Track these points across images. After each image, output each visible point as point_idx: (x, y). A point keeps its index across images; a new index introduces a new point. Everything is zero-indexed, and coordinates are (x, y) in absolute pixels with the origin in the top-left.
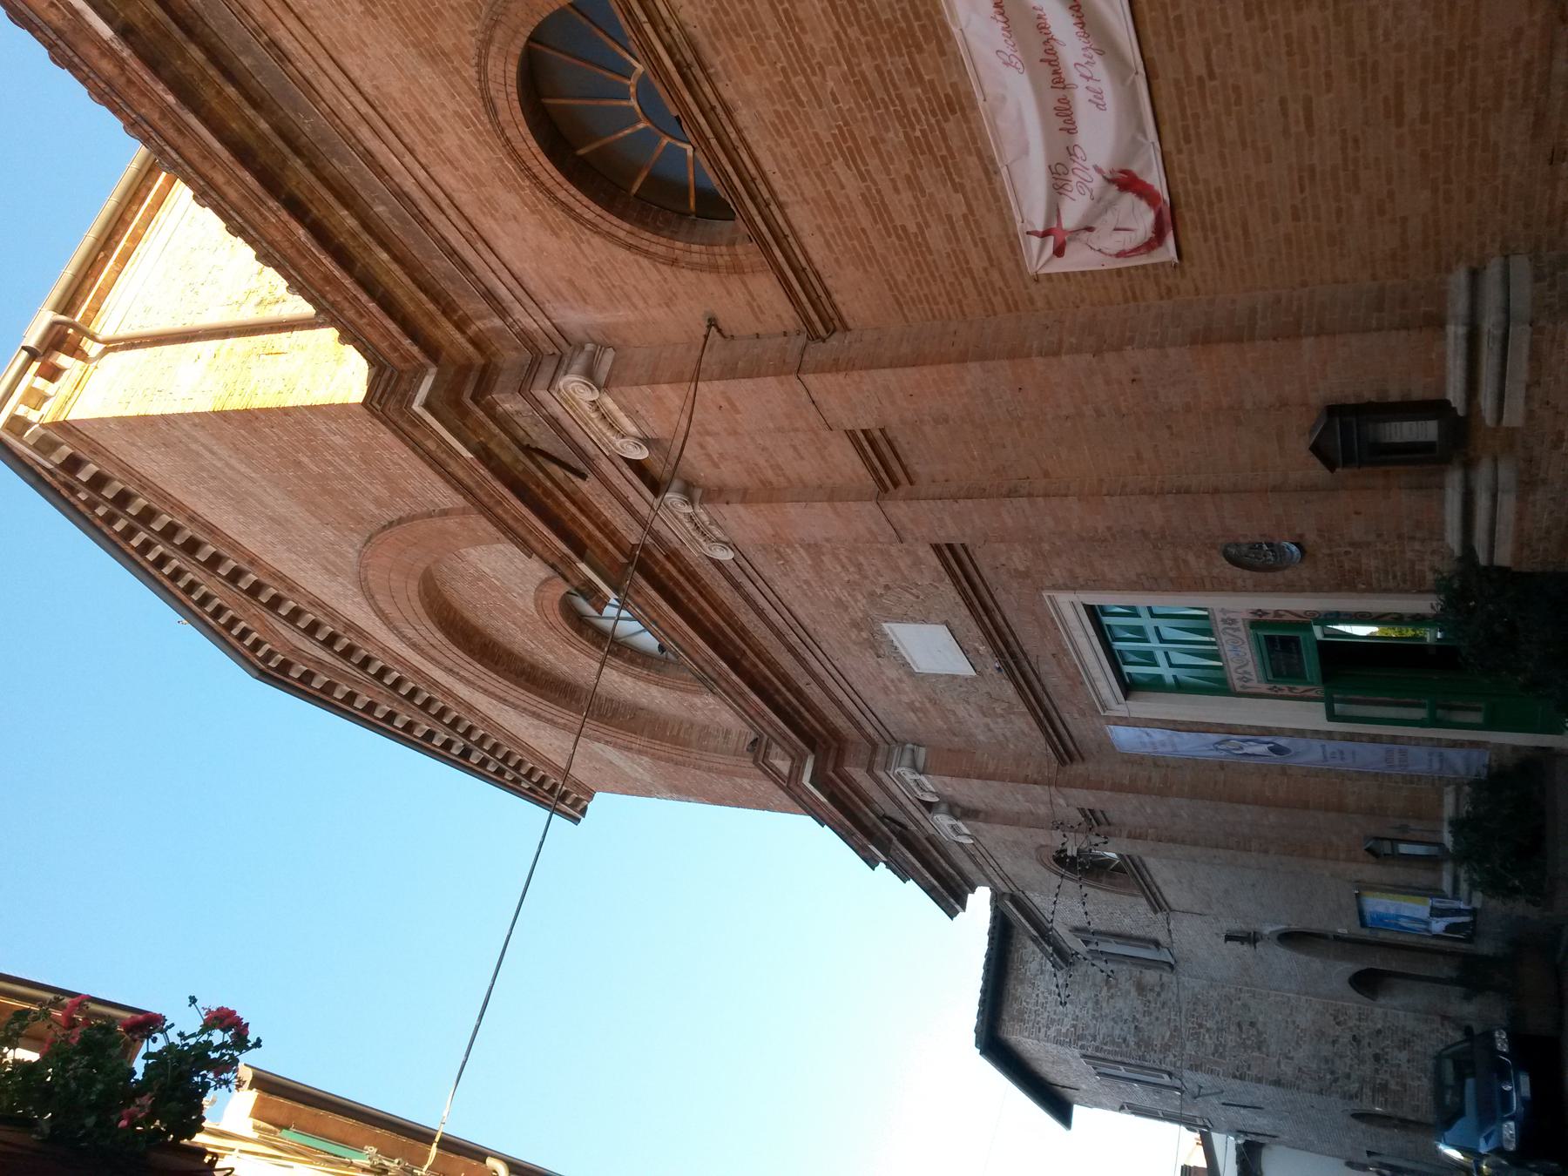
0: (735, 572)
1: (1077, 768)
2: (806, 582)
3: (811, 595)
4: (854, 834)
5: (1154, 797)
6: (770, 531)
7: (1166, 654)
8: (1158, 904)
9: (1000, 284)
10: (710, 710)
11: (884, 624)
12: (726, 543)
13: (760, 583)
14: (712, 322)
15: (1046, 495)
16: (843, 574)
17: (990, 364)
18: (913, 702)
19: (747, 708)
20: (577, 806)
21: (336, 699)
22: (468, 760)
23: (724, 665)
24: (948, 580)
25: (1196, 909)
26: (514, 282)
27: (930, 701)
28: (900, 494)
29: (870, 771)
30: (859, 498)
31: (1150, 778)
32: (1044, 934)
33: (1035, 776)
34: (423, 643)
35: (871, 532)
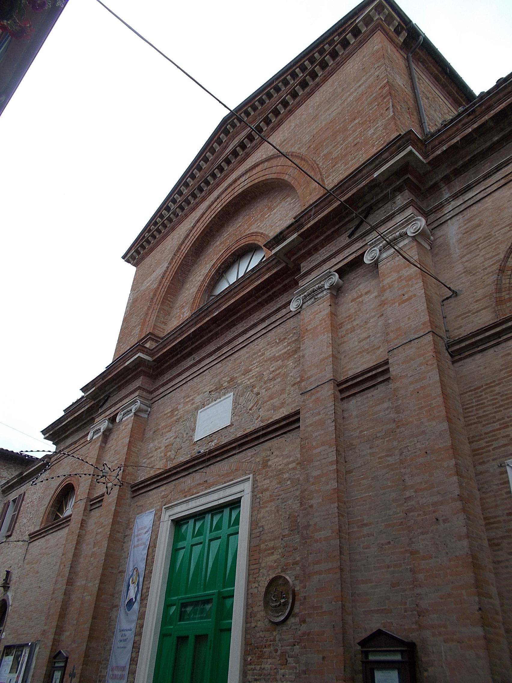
0: (284, 311)
1: (129, 495)
2: (263, 354)
3: (254, 357)
4: (103, 380)
5: (109, 533)
6: (309, 327)
7: (201, 543)
8: (34, 536)
9: (496, 444)
10: (180, 315)
11: (233, 393)
12: (301, 307)
13: (264, 331)
14: (455, 294)
15: (338, 471)
16: (268, 371)
17: (447, 435)
18: (178, 410)
19: (187, 326)
20: (131, 258)
21: (207, 153)
22: (164, 209)
23: (216, 314)
24: (262, 424)
25: (28, 556)
26: (478, 199)
27: (178, 419)
28: (336, 392)
29: (139, 388)
30: (335, 371)
31: (119, 532)
32: (22, 480)
33: (127, 471)
34: (236, 184)
35: (309, 378)
